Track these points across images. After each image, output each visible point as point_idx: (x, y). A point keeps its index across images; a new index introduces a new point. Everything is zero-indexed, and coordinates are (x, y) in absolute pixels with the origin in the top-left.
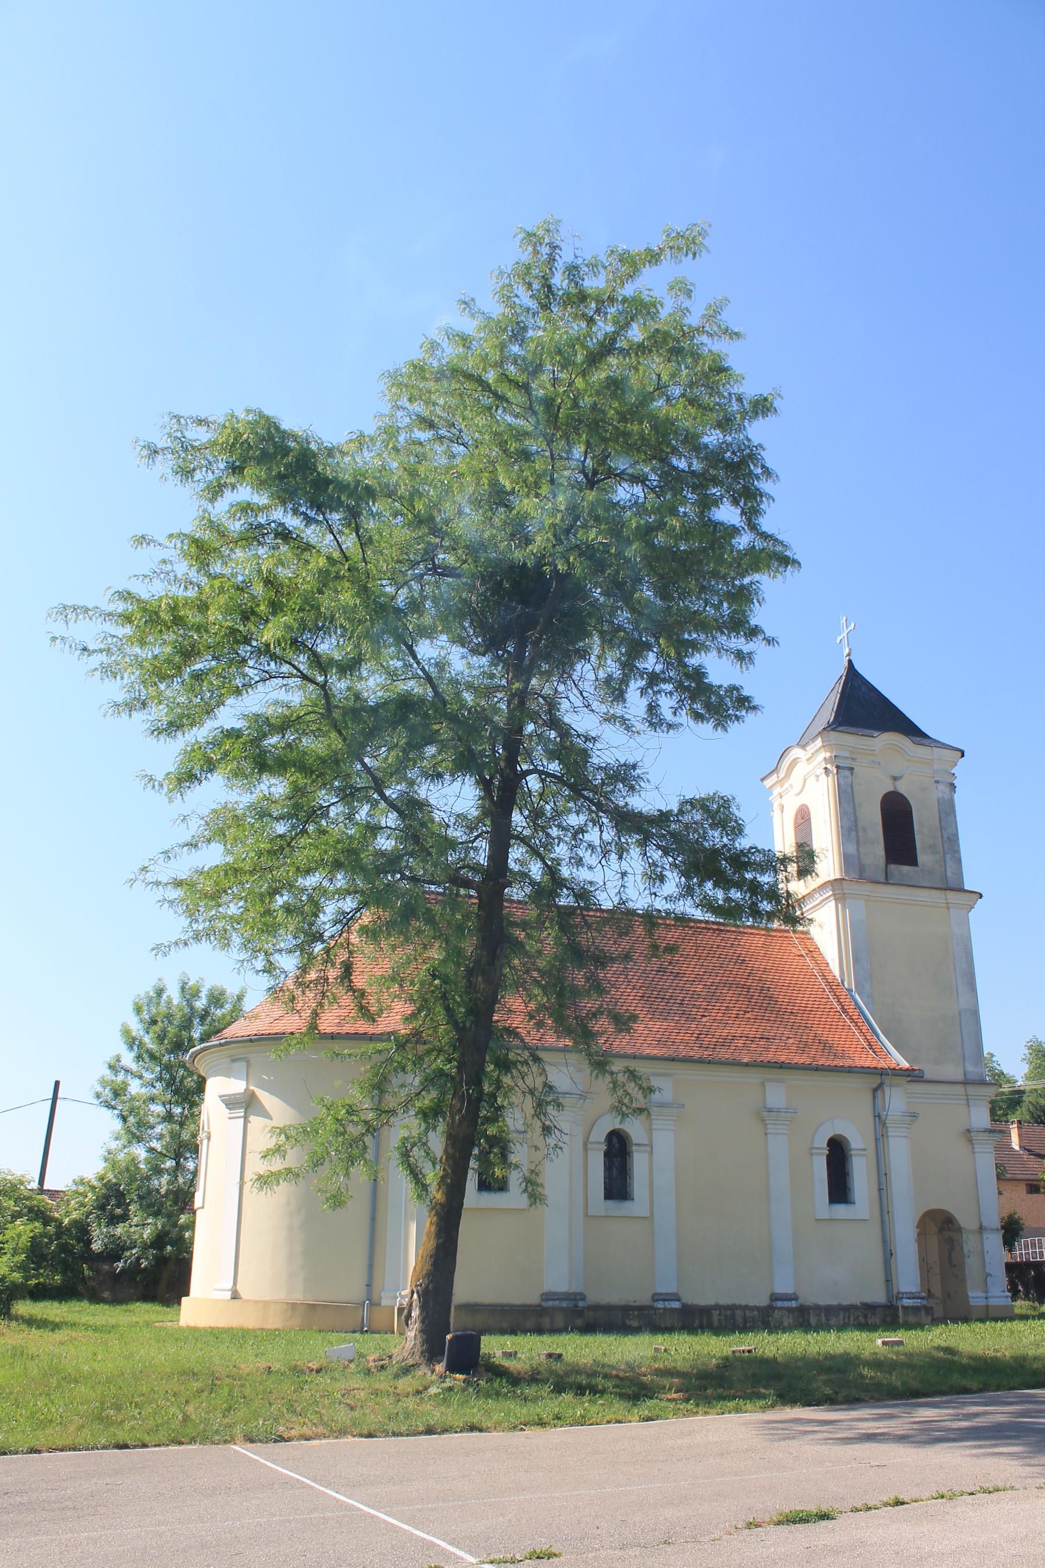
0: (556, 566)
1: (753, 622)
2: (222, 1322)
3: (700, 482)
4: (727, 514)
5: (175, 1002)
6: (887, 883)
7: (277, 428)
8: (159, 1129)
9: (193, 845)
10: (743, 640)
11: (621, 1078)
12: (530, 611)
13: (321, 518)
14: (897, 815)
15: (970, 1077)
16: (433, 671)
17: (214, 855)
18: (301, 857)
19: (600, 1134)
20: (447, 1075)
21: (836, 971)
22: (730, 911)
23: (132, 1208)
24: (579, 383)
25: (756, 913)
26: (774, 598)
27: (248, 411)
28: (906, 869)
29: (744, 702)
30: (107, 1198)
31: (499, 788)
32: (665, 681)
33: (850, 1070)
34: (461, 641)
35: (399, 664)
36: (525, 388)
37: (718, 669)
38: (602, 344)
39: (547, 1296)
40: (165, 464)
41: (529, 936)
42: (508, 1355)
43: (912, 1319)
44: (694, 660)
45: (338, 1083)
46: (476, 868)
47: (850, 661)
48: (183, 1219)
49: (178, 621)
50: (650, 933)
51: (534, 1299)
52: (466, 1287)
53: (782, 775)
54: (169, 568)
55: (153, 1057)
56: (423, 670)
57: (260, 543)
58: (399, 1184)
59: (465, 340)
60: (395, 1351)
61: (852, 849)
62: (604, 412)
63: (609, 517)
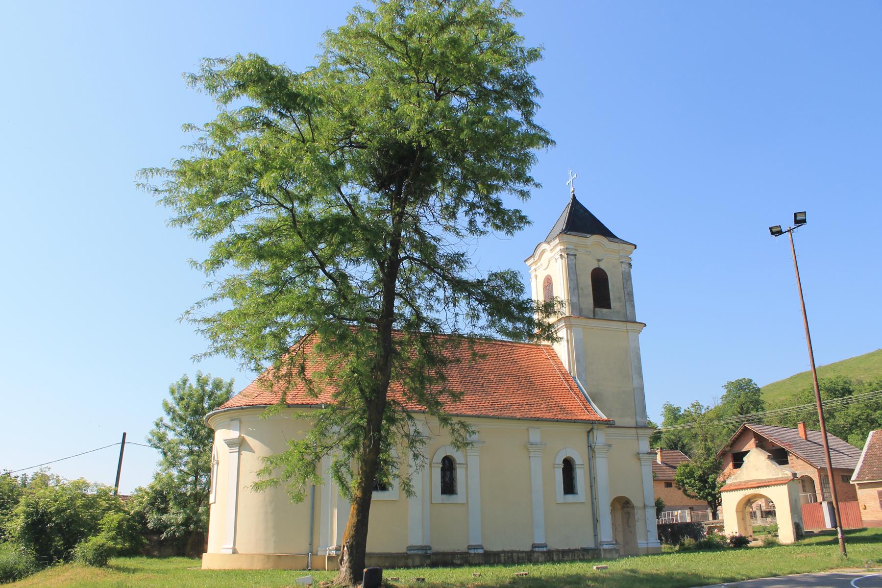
0: (420, 143)
1: (528, 175)
2: (228, 566)
3: (500, 96)
4: (515, 114)
5: (194, 387)
6: (594, 318)
7: (266, 64)
8: (185, 459)
9: (214, 299)
10: (522, 184)
11: (457, 427)
12: (405, 169)
13: (289, 114)
14: (599, 279)
15: (639, 424)
16: (351, 201)
17: (227, 305)
18: (279, 307)
19: (438, 459)
20: (362, 427)
21: (567, 367)
22: (516, 335)
23: (171, 504)
24: (434, 40)
25: (531, 336)
26: (542, 163)
27: (250, 55)
28: (604, 310)
29: (523, 219)
30: (155, 499)
31: (388, 267)
32: (479, 207)
33: (575, 421)
34: (365, 185)
35: (333, 198)
36: (404, 43)
37: (508, 200)
38: (448, 19)
39: (410, 548)
40: (200, 85)
41: (403, 349)
42: (397, 580)
43: (608, 556)
44: (494, 196)
45: (300, 432)
46: (374, 312)
47: (574, 195)
48: (201, 509)
49: (211, 174)
50: (471, 348)
51: (403, 550)
52: (373, 545)
53: (536, 258)
54: (204, 142)
55: (181, 418)
56: (346, 200)
57: (254, 128)
58: (330, 488)
59: (371, 16)
60: (335, 579)
61: (575, 300)
62: (448, 57)
63: (447, 114)
